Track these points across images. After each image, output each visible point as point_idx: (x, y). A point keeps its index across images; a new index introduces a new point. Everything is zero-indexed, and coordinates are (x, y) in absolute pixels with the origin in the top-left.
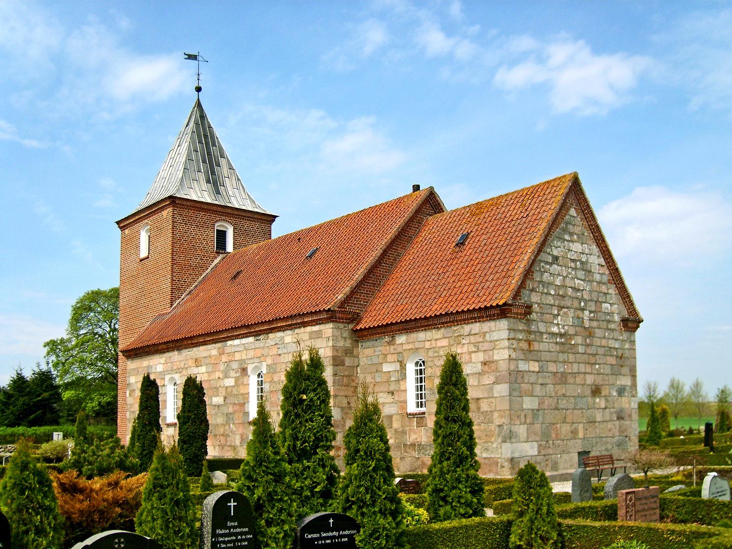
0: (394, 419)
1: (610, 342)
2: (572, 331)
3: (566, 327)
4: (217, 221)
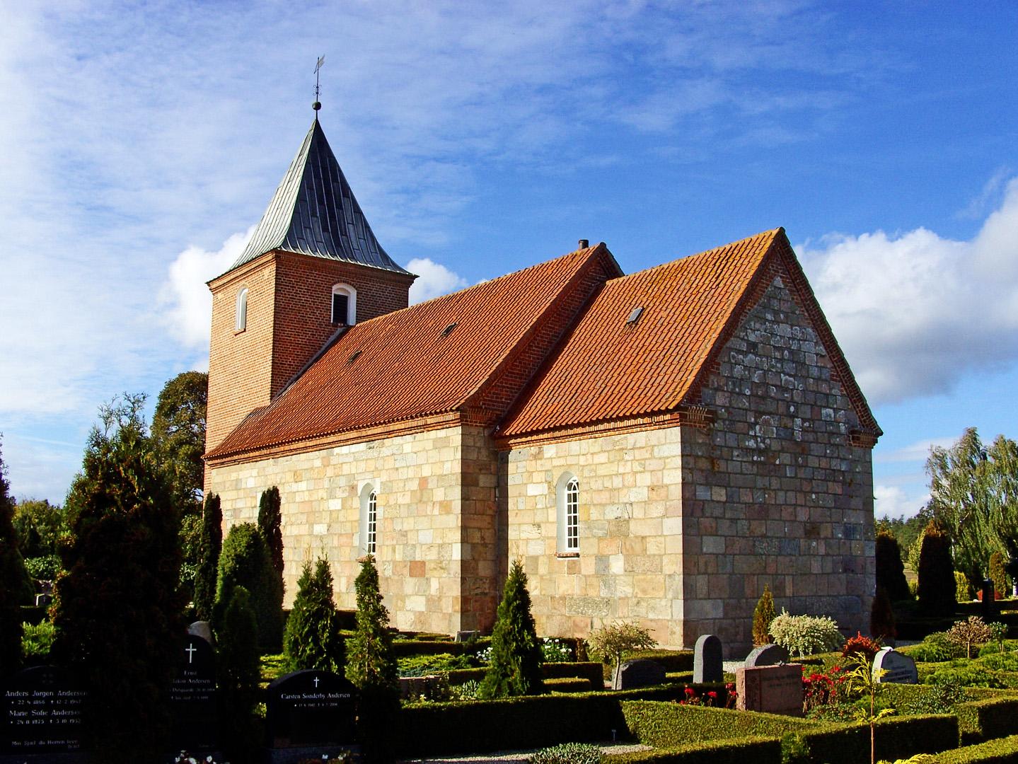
0: (541, 560)
1: (834, 462)
2: (775, 446)
3: (768, 441)
4: (335, 283)
